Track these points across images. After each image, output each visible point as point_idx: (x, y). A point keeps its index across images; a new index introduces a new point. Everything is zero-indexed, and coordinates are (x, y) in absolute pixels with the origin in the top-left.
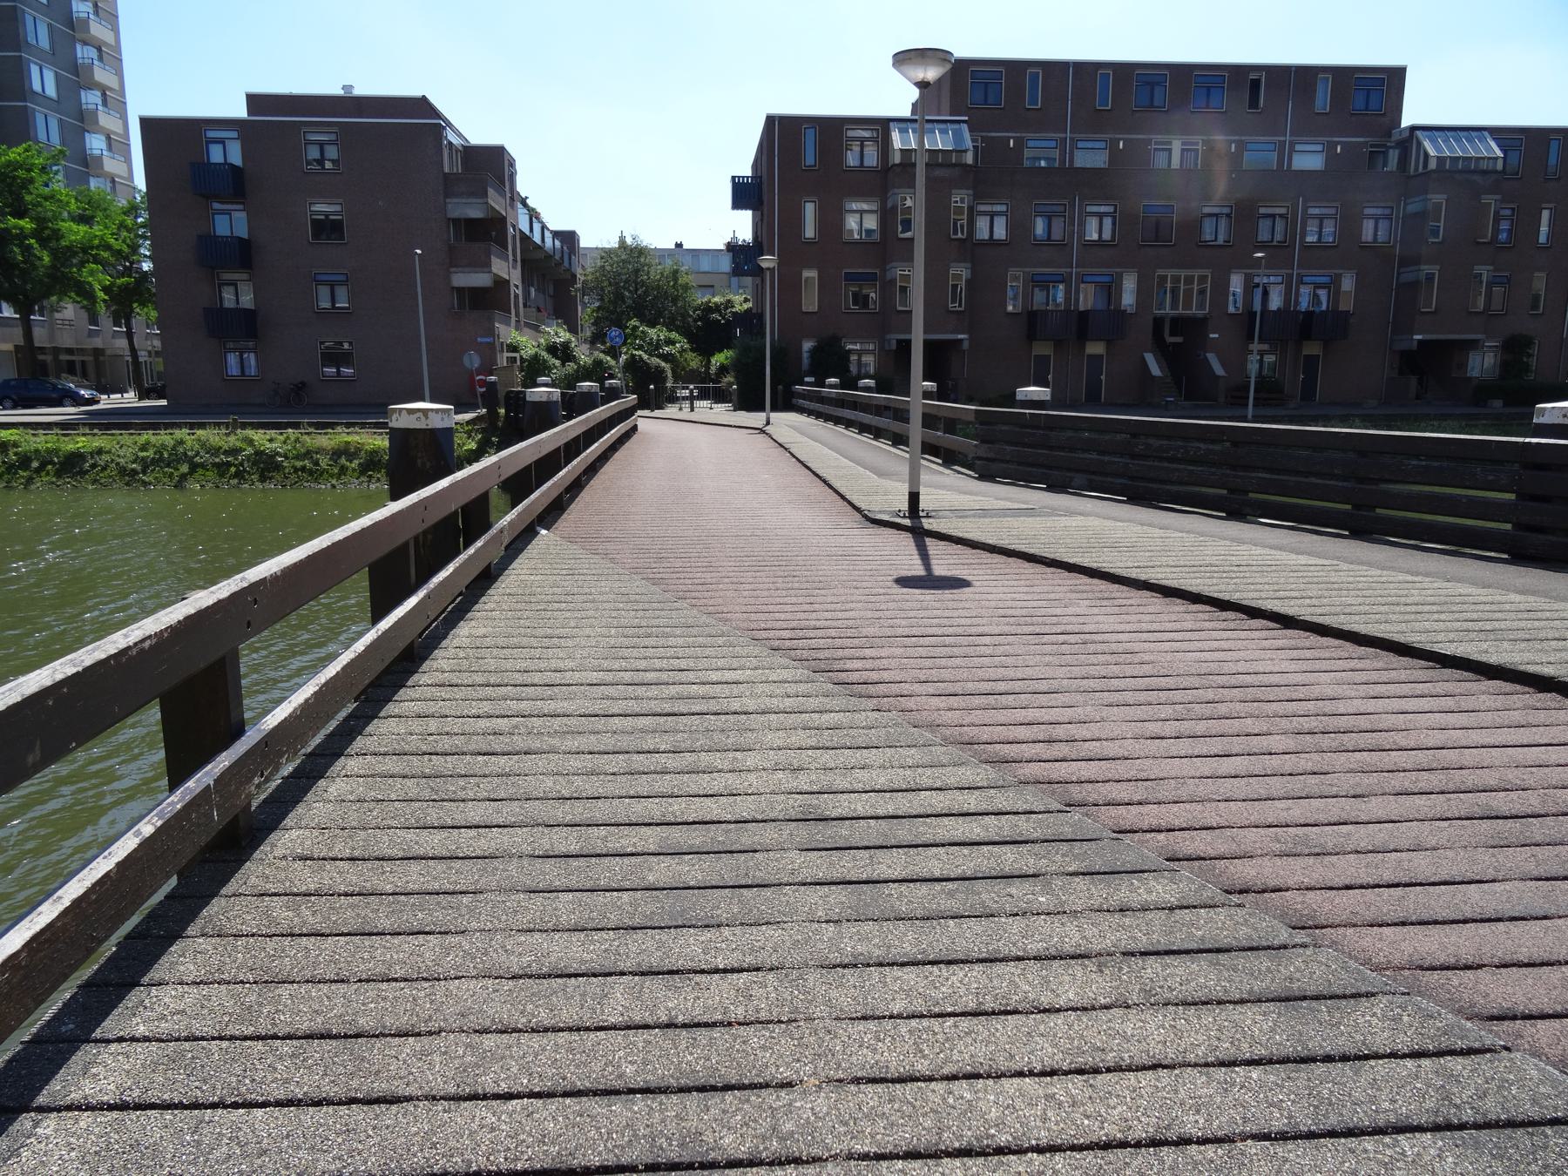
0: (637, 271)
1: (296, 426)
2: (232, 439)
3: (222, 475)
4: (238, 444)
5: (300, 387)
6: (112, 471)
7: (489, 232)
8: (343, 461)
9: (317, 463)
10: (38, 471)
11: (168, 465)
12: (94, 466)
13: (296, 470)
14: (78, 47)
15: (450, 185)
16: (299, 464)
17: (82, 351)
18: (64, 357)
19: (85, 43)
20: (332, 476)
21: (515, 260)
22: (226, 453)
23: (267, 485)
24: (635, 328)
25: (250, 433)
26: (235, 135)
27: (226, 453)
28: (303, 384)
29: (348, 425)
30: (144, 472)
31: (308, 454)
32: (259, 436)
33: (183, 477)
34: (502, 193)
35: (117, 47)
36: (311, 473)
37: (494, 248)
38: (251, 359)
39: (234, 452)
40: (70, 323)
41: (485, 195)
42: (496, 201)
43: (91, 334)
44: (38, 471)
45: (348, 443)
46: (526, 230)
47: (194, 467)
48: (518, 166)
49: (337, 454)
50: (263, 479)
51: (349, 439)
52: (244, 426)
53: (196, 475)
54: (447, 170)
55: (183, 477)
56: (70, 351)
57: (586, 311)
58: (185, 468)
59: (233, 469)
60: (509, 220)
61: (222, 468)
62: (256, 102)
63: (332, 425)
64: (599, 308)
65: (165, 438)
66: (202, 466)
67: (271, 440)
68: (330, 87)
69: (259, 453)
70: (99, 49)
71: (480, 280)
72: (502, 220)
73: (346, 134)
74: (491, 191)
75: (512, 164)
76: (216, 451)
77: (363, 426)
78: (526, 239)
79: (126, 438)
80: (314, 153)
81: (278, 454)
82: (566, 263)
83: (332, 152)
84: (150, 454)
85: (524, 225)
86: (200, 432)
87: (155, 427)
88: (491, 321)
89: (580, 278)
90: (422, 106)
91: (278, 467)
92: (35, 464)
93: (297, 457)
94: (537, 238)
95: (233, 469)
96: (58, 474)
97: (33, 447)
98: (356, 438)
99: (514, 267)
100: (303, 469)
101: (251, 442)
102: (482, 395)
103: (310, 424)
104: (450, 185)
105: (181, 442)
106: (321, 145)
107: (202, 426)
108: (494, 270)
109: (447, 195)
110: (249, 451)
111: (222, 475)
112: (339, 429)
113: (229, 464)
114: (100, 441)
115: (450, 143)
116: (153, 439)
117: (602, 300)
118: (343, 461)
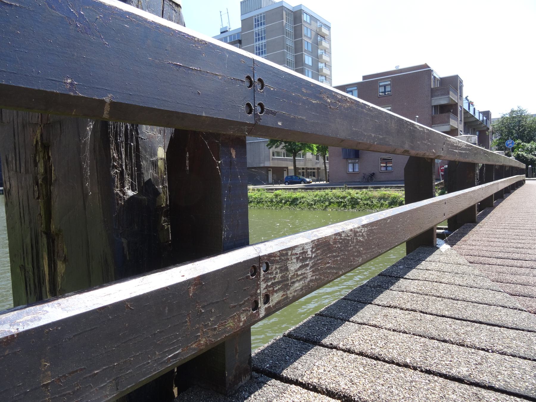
0: (520, 121)
1: (366, 188)
2: (344, 193)
3: (339, 206)
4: (346, 195)
5: (373, 175)
6: (305, 204)
7: (449, 109)
8: (382, 201)
9: (372, 202)
10: (285, 203)
11: (322, 202)
12: (300, 202)
13: (365, 205)
14: (320, 77)
15: (433, 92)
16: (366, 202)
17: (314, 169)
18: (309, 171)
19: (322, 76)
20: (377, 207)
21: (461, 120)
22: (342, 198)
23: (353, 210)
24: (519, 144)
25: (350, 191)
26: (356, 88)
27: (342, 198)
28: (374, 174)
29: (386, 187)
30: (315, 205)
31: (369, 198)
32: (353, 192)
33: (326, 207)
34: (456, 93)
35: (331, 75)
36: (370, 205)
37: (451, 115)
38: (357, 166)
39: (344, 198)
40: (311, 160)
41: (449, 94)
42: (453, 96)
43: (316, 163)
44: (285, 203)
45: (385, 194)
46: (467, 109)
47: (330, 203)
48: (464, 83)
49: (380, 198)
50: (353, 208)
51: (385, 193)
52: (349, 188)
53: (331, 206)
54: (432, 87)
55: (326, 207)
56: (311, 169)
57: (494, 139)
58: (327, 203)
59: (343, 204)
60: (459, 104)
61: (339, 203)
62: (365, 77)
63: (379, 188)
64: (500, 139)
65: (322, 193)
66: (333, 203)
67: (357, 193)
68: (393, 68)
69: (352, 198)
70: (326, 77)
71: (443, 101)
72: (456, 104)
73: (393, 80)
74: (451, 93)
75: (461, 82)
76: (338, 197)
77: (391, 187)
78: (466, 113)
79: (311, 193)
80: (382, 89)
81: (359, 198)
82: (485, 123)
83: (388, 89)
84: (317, 198)
85: (466, 106)
86: (334, 191)
87: (320, 189)
88: (449, 118)
89: (491, 128)
90: (426, 66)
91: (358, 203)
92: (283, 201)
93: (365, 200)
94: (472, 112)
95: (343, 204)
96: (290, 205)
97: (284, 196)
98: (388, 192)
99: (461, 124)
100: (367, 204)
101: (350, 194)
102: (442, 175)
103: (372, 187)
104: (433, 92)
105: (327, 194)
106: (385, 86)
107: (335, 188)
108: (451, 124)
109: (432, 97)
110: (349, 197)
111: (339, 206)
112: (382, 189)
113: (341, 202)
114: (303, 194)
115: (435, 77)
116: (319, 193)
117: (501, 135)
118: (382, 201)
